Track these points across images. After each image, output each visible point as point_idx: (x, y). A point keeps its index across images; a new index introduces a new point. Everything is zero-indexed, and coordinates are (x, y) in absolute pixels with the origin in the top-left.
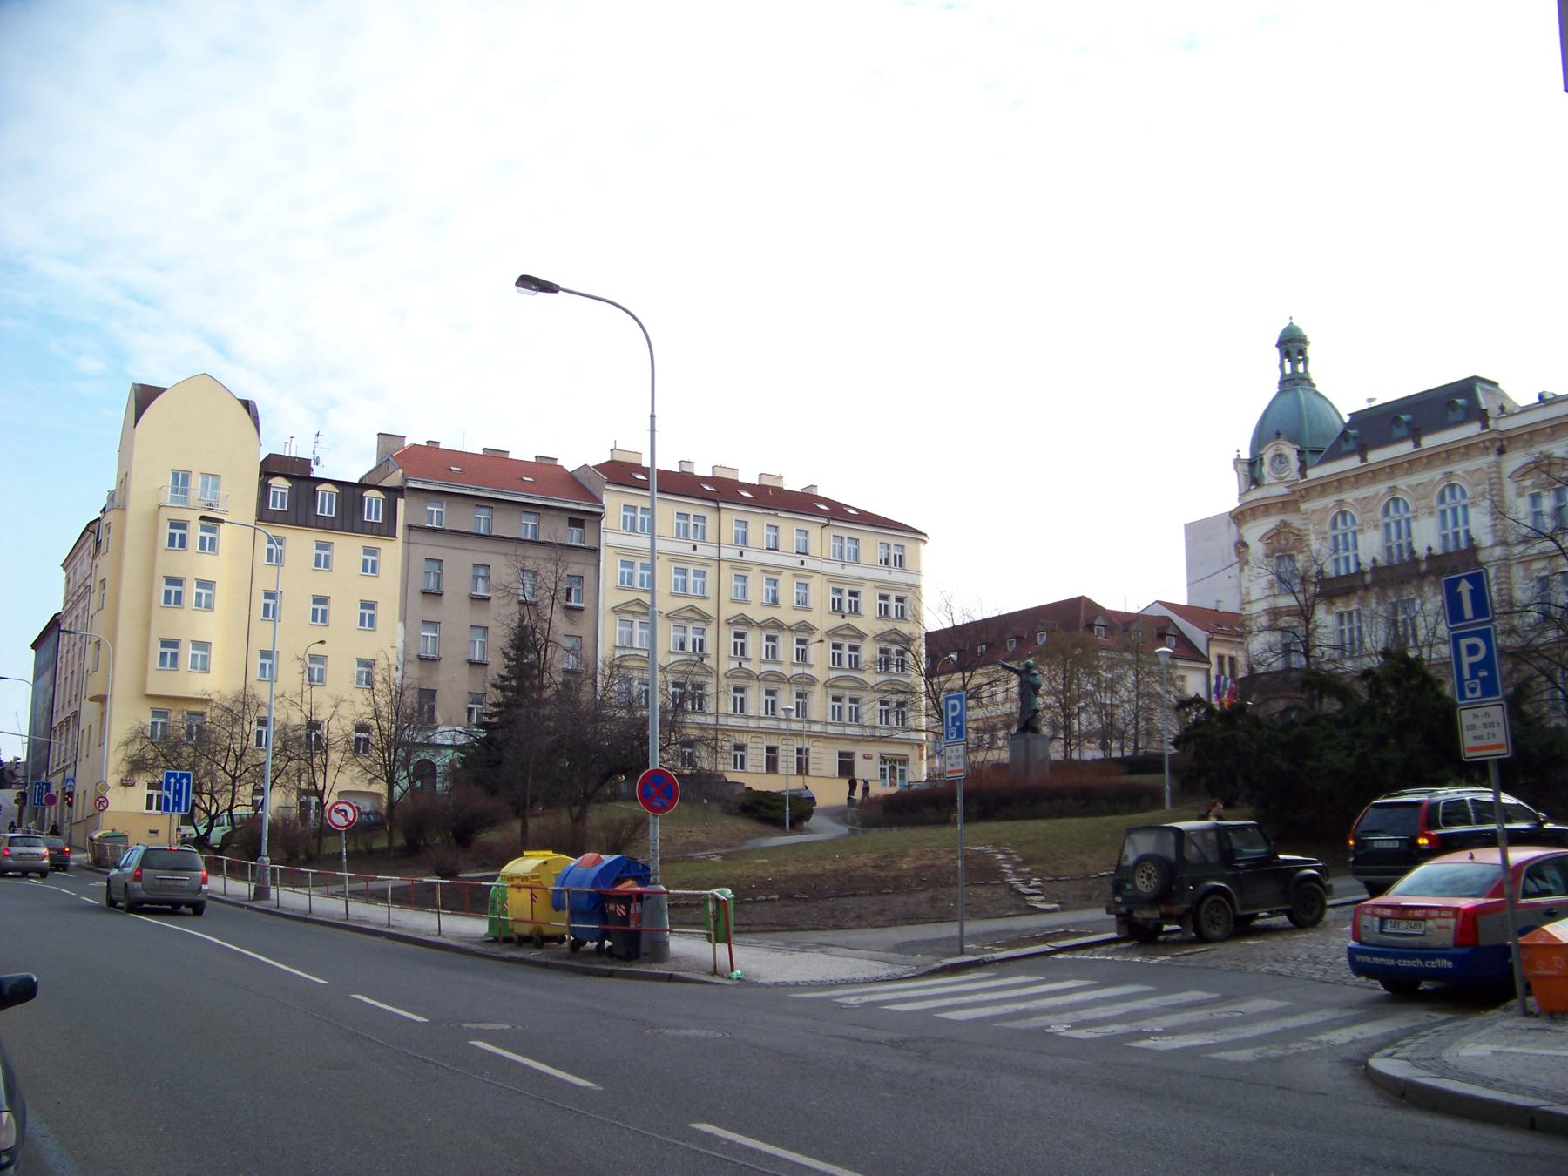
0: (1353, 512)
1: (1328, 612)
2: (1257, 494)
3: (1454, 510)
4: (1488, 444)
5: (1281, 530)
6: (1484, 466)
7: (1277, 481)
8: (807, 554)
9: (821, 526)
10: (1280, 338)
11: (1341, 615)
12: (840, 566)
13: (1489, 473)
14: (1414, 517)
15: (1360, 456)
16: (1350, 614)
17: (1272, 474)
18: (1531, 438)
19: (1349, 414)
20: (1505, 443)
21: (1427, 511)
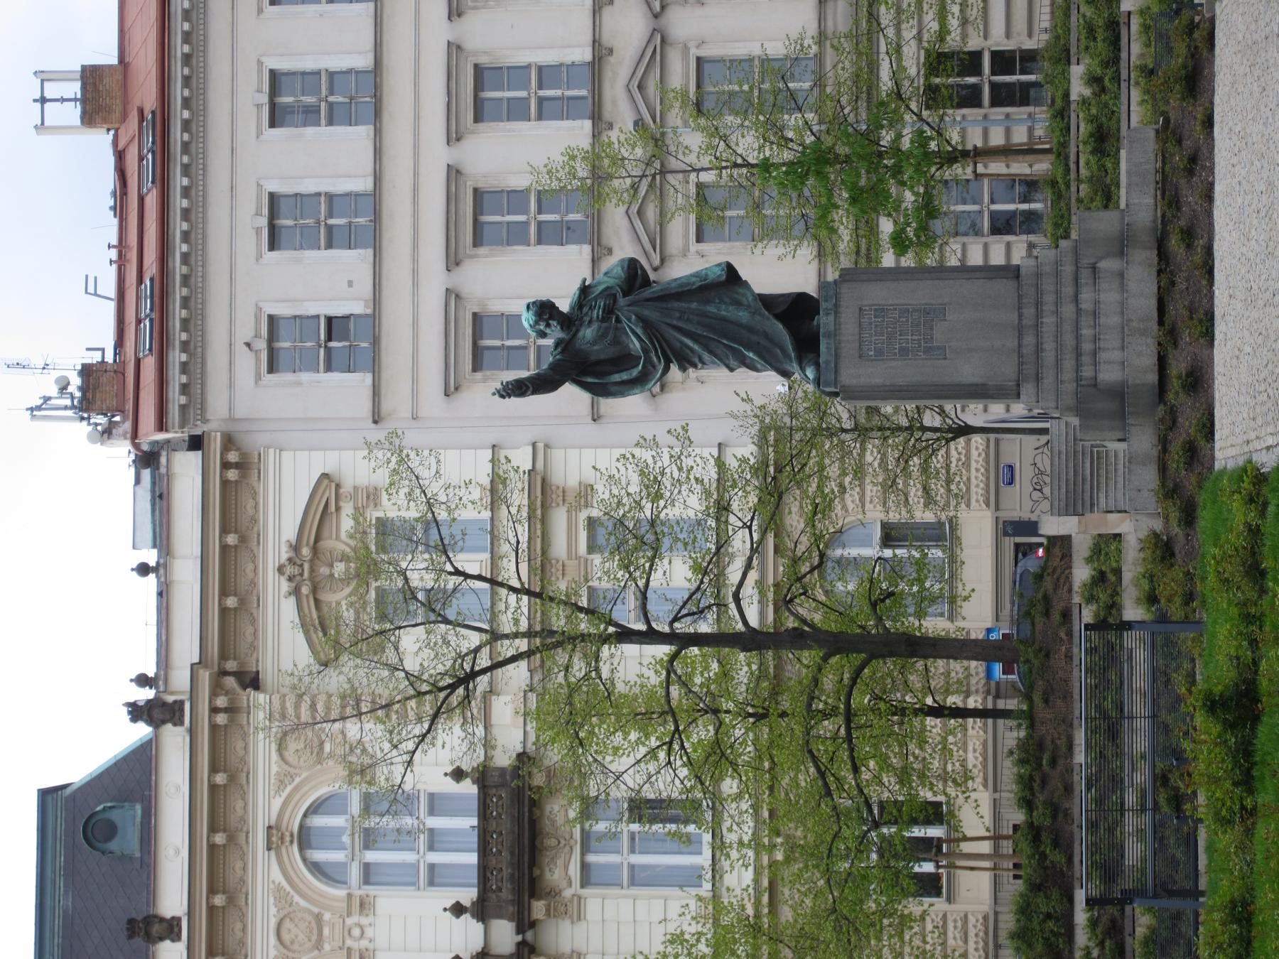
4: (221, 702)
20: (231, 665)
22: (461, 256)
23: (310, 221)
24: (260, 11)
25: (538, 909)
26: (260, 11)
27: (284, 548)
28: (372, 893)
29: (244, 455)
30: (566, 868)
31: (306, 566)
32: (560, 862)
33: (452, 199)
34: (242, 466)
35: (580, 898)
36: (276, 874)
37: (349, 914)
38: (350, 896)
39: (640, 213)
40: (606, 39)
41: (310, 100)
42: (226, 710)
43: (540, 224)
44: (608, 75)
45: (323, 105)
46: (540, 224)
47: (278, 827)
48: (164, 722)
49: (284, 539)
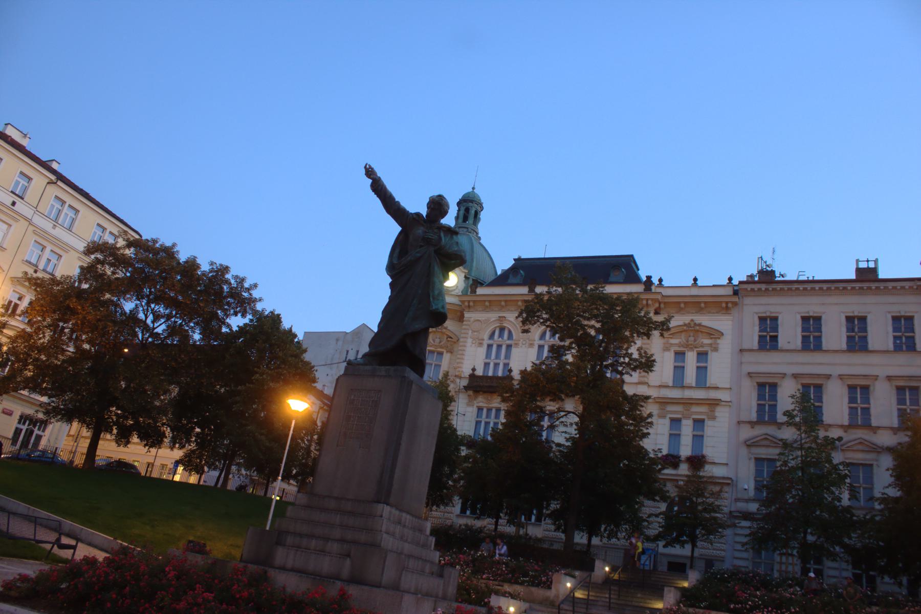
0: (509, 327)
1: (470, 404)
3: (499, 346)
4: (471, 304)
8: (22, 198)
9: (47, 181)
10: (464, 196)
11: (480, 409)
12: (52, 225)
14: (516, 344)
15: (529, 287)
16: (489, 410)
20: (662, 306)
21: (478, 341)
23: (768, 330)
24: (889, 312)
26: (889, 312)
27: (699, 322)
30: (483, 402)
31: (693, 329)
32: (483, 400)
33: (818, 376)
34: (727, 308)
35: (473, 405)
36: (494, 319)
37: (529, 340)
39: (766, 439)
40: (880, 432)
41: (856, 330)
43: (764, 405)
46: (764, 405)
47: (505, 320)
48: (645, 286)
49: (703, 322)
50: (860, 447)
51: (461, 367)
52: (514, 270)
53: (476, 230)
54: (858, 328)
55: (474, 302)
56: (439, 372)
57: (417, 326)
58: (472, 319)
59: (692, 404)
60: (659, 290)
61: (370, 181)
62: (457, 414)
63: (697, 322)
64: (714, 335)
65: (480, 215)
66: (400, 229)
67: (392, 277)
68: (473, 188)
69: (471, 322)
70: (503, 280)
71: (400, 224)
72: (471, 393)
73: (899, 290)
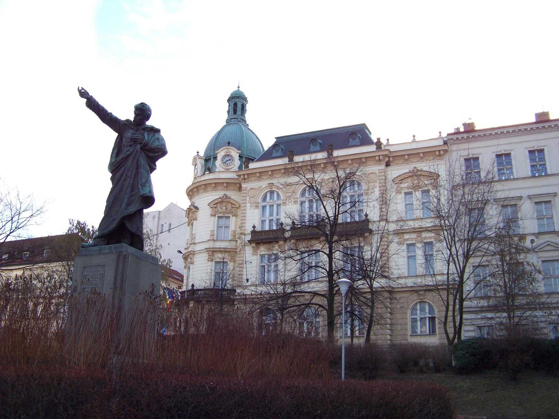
1: (255, 253)
2: (209, 176)
3: (271, 206)
4: (381, 158)
5: (224, 200)
6: (377, 171)
7: (223, 170)
11: (262, 256)
13: (379, 176)
15: (328, 152)
17: (221, 165)
18: (227, 187)
19: (276, 138)
20: (391, 159)
22: (532, 199)
24: (526, 148)
25: (254, 245)
26: (526, 148)
27: (421, 168)
28: (298, 203)
29: (442, 155)
30: (264, 251)
32: (264, 249)
34: (440, 155)
36: (264, 186)
37: (294, 199)
38: (259, 203)
42: (379, 159)
44: (551, 236)
45: (536, 163)
48: (377, 145)
50: (549, 248)
51: (244, 226)
52: (275, 146)
53: (244, 119)
54: (539, 158)
55: (248, 174)
56: (229, 232)
57: (131, 210)
58: (248, 188)
59: (403, 233)
60: (387, 148)
61: (85, 100)
62: (246, 263)
63: (419, 169)
64: (235, 205)
65: (246, 107)
66: (116, 135)
67: (112, 172)
68: (239, 87)
69: (248, 191)
70: (268, 155)
71: (115, 130)
72: (254, 245)
73: (535, 129)
